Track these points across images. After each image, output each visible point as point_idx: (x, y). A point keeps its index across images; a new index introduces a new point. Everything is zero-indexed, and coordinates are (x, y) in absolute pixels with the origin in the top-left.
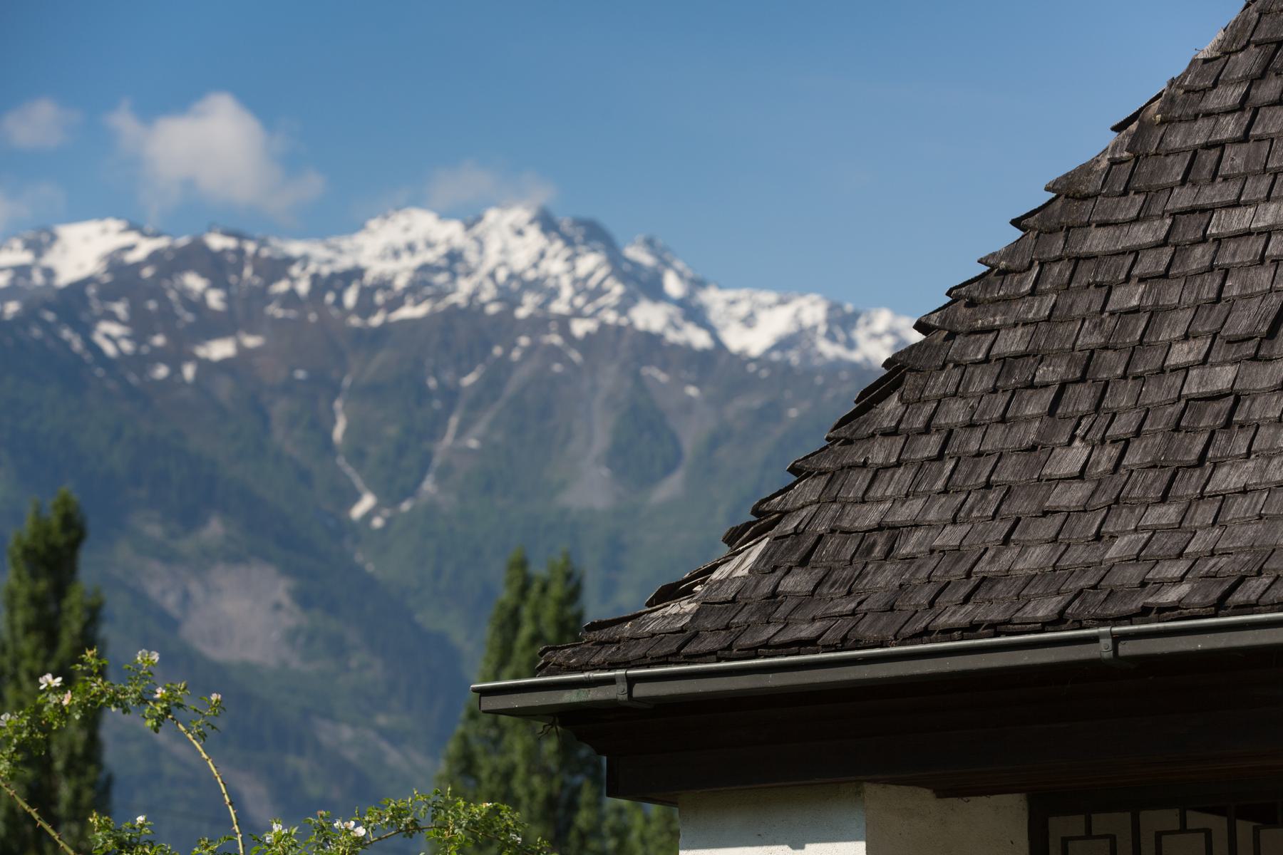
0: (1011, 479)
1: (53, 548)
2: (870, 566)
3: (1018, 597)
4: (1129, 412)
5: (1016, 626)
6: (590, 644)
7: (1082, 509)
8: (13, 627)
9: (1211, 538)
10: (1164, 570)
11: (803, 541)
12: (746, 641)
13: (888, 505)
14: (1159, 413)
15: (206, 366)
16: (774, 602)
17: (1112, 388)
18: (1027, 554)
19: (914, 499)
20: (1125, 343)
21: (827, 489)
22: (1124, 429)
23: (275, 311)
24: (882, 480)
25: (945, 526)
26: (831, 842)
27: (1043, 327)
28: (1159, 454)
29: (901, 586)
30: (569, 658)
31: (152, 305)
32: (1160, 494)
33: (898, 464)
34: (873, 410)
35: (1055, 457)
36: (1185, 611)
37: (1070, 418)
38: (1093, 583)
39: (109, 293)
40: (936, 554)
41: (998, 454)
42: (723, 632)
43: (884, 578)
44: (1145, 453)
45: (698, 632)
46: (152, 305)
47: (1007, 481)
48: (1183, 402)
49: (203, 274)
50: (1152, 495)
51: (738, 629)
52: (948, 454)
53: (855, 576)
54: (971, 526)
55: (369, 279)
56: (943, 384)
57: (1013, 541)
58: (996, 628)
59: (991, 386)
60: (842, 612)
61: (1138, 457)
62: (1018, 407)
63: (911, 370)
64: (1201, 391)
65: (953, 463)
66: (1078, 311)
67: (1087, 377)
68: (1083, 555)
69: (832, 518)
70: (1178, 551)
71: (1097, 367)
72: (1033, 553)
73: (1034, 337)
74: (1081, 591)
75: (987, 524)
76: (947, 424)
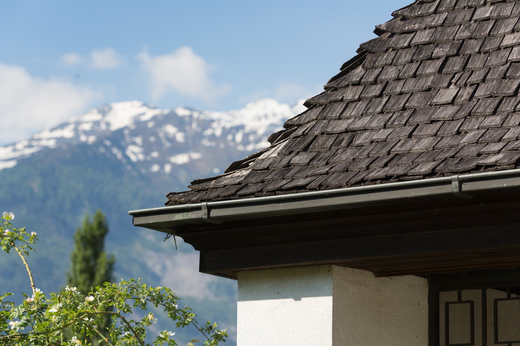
0: (416, 105)
1: (93, 236)
2: (340, 150)
3: (413, 163)
4: (480, 70)
5: (410, 177)
6: (193, 191)
7: (451, 119)
8: (75, 271)
9: (517, 131)
10: (491, 147)
11: (307, 139)
12: (270, 187)
13: (352, 120)
14: (496, 70)
15: (175, 167)
16: (288, 169)
17: (473, 58)
18: (420, 142)
19: (365, 116)
20: (481, 35)
21: (322, 113)
22: (477, 78)
23: (206, 143)
24: (350, 108)
25: (380, 129)
26: (315, 297)
27: (439, 29)
28: (494, 90)
29: (354, 159)
30: (181, 198)
31: (152, 139)
32: (493, 110)
33: (359, 100)
34: (349, 74)
35: (440, 94)
36: (499, 167)
37: (450, 74)
38: (452, 154)
39: (134, 133)
40: (374, 144)
41: (410, 93)
42: (260, 184)
43: (346, 156)
44: (487, 90)
45: (247, 184)
46: (152, 139)
47: (413, 106)
48: (509, 64)
49: (175, 126)
50: (489, 111)
51: (268, 182)
52: (385, 94)
53: (331, 155)
54: (393, 129)
55: (247, 129)
56: (386, 59)
57: (414, 136)
58: (399, 178)
59: (410, 59)
60: (322, 172)
61: (483, 92)
62: (423, 69)
63: (370, 53)
64: (518, 57)
65: (387, 98)
66: (458, 20)
67: (460, 53)
68: (450, 142)
69: (323, 127)
70: (499, 138)
71: (466, 48)
72: (424, 141)
73: (434, 34)
74: (446, 159)
75: (402, 128)
76: (386, 79)
